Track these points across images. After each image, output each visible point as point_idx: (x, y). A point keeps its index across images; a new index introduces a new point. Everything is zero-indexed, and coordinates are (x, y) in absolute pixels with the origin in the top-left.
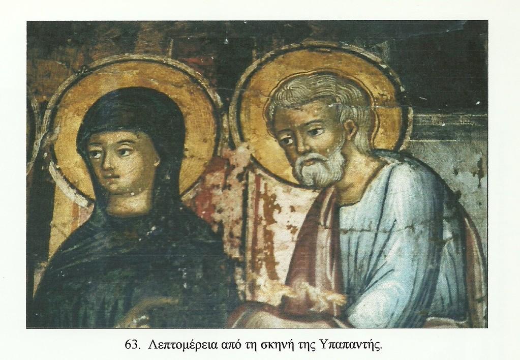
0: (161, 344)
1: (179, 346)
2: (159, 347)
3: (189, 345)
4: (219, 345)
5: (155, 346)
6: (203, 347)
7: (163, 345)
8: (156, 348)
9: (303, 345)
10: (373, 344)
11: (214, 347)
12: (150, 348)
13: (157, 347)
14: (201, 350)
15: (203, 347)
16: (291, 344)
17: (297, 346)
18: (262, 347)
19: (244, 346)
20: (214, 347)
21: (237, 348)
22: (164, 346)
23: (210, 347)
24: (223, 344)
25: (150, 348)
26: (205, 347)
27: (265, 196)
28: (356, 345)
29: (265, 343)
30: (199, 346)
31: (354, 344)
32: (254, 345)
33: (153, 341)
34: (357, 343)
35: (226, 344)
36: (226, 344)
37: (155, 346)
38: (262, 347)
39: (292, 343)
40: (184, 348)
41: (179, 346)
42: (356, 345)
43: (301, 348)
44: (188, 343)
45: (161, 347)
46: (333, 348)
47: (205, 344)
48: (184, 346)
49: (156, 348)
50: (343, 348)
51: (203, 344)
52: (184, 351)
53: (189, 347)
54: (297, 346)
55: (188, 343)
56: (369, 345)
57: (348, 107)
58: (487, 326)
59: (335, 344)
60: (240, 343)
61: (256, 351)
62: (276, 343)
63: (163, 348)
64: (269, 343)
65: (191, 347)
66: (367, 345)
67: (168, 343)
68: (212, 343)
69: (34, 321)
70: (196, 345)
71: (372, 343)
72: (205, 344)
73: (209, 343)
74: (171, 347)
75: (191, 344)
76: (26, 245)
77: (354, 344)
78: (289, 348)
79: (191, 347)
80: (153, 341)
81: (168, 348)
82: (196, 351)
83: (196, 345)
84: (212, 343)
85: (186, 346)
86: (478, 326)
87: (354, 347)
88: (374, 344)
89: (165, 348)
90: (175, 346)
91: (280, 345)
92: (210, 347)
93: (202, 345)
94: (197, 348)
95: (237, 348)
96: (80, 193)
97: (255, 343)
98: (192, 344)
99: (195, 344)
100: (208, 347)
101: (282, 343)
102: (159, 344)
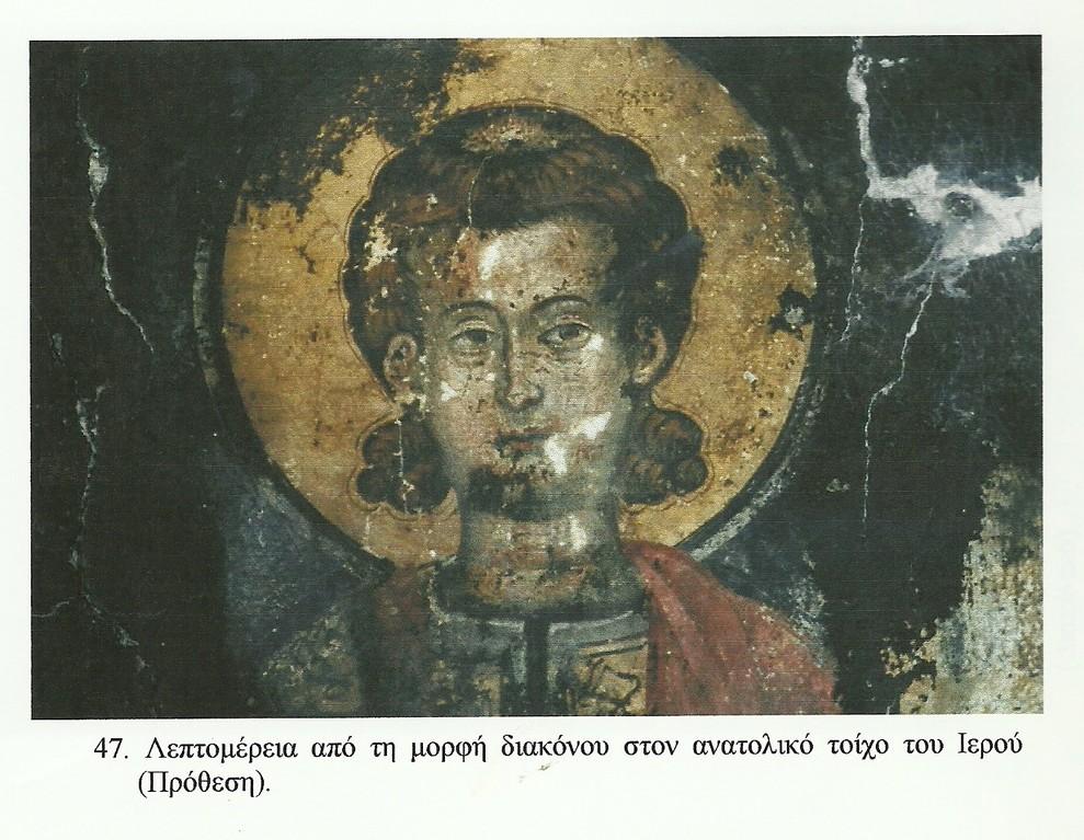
0: (173, 747)
1: (213, 751)
3: (235, 750)
6: (265, 753)
7: (177, 748)
8: (162, 756)
9: (381, 749)
10: (599, 752)
11: (727, 751)
12: (148, 756)
13: (165, 754)
15: (214, 788)
16: (480, 747)
18: (627, 752)
20: (727, 751)
21: (751, 752)
22: (179, 751)
23: (522, 751)
24: (314, 746)
25: (148, 756)
26: (269, 753)
28: (707, 747)
29: (632, 742)
30: (256, 750)
31: (704, 745)
32: (390, 748)
33: (155, 741)
34: (710, 742)
35: (732, 744)
36: (732, 744)
38: (886, 743)
39: (482, 743)
41: (213, 751)
42: (707, 747)
43: (909, 751)
44: (231, 745)
45: (173, 754)
47: (269, 747)
49: (162, 756)
50: (329, 755)
52: (223, 761)
53: (234, 752)
57: (794, 287)
59: (649, 746)
60: (352, 745)
61: (484, 760)
64: (788, 742)
65: (238, 753)
67: (189, 746)
68: (285, 746)
69: (39, 712)
72: (269, 747)
73: (278, 745)
74: (196, 754)
75: (238, 746)
76: (29, 364)
77: (704, 745)
78: (477, 754)
79: (238, 753)
80: (155, 741)
81: (189, 756)
82: (251, 761)
84: (285, 746)
85: (228, 752)
87: (703, 751)
88: (333, 753)
92: (282, 752)
94: (982, 751)
95: (751, 752)
97: (391, 743)
98: (242, 747)
100: (276, 752)
101: (668, 742)
102: (169, 747)
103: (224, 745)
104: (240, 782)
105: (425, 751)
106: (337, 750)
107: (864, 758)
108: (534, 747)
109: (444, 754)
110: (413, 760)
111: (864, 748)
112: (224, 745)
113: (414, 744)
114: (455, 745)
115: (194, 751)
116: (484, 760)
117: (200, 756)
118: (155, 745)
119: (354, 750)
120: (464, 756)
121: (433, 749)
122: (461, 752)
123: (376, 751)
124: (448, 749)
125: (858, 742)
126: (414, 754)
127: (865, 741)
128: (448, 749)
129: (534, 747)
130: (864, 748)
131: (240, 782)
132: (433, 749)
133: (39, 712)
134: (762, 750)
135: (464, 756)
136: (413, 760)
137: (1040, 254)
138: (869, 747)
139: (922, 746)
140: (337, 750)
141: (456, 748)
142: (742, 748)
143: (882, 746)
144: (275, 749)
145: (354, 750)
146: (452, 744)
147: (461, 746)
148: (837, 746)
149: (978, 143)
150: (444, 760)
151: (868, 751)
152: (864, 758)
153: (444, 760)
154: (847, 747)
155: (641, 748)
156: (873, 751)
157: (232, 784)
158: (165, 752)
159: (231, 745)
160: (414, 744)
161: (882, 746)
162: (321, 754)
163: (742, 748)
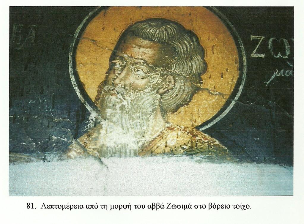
0: (49, 206)
1: (60, 207)
2: (47, 208)
3: (66, 207)
4: (193, 207)
5: (45, 207)
8: (46, 208)
9: (103, 207)
12: (42, 208)
13: (46, 208)
14: (73, 210)
15: (74, 208)
16: (130, 206)
17: (133, 207)
18: (195, 208)
19: (100, 207)
21: (95, 208)
22: (50, 207)
23: (79, 207)
25: (42, 208)
26: (222, 207)
27: (191, 70)
29: (197, 205)
30: (72, 207)
32: (106, 206)
33: (44, 204)
37: (45, 207)
38: (195, 208)
40: (63, 208)
41: (60, 207)
43: (102, 208)
44: (185, 205)
45: (49, 208)
46: (93, 208)
47: (222, 206)
48: (63, 207)
50: (91, 208)
51: (221, 206)
52: (62, 210)
53: (66, 207)
54: (133, 207)
55: (185, 205)
56: (105, 206)
58: (9, 196)
59: (57, 207)
61: (131, 210)
62: (105, 205)
63: (50, 208)
65: (67, 207)
66: (103, 207)
67: (53, 205)
68: (80, 205)
69: (14, 10)
70: (70, 206)
71: (131, 205)
72: (75, 206)
73: (78, 205)
75: (67, 206)
76: (294, 149)
78: (129, 208)
79: (67, 207)
80: (44, 204)
81: (53, 208)
82: (70, 210)
83: (70, 206)
84: (80, 205)
85: (64, 207)
86: (9, 193)
89: (51, 208)
90: (57, 207)
91: (125, 207)
92: (79, 207)
93: (74, 207)
94: (71, 208)
96: (197, 58)
97: (106, 205)
98: (68, 206)
99: (70, 205)
102: (47, 206)
103: (63, 205)
104: (181, 206)
105: (128, 206)
106: (92, 207)
107: (243, 210)
108: (89, 206)
109: (217, 208)
110: (111, 210)
111: (242, 207)
112: (63, 205)
113: (111, 205)
114: (123, 206)
115: (54, 207)
116: (131, 210)
117: (56, 208)
118: (44, 205)
119: (205, 207)
120: (125, 209)
121: (116, 207)
122: (124, 207)
123: (102, 207)
124: (121, 207)
125: (241, 205)
126: (111, 208)
127: (243, 205)
128: (121, 207)
129: (89, 206)
130: (242, 207)
131: (181, 206)
132: (116, 207)
133: (14, 10)
134: (246, 206)
135: (125, 209)
136: (111, 210)
137: (10, 152)
138: (244, 207)
139: (139, 207)
140: (92, 207)
141: (123, 206)
142: (56, 207)
143: (248, 207)
144: (77, 206)
145: (205, 207)
146: (122, 206)
147: (124, 206)
148: (136, 206)
149: (103, 142)
150: (119, 210)
151: (244, 208)
152: (243, 210)
153: (119, 210)
154: (238, 207)
155: (199, 207)
156: (245, 208)
157: (179, 207)
158: (46, 207)
159: (65, 205)
160: (111, 205)
161: (248, 207)
162: (89, 208)
163: (56, 207)
